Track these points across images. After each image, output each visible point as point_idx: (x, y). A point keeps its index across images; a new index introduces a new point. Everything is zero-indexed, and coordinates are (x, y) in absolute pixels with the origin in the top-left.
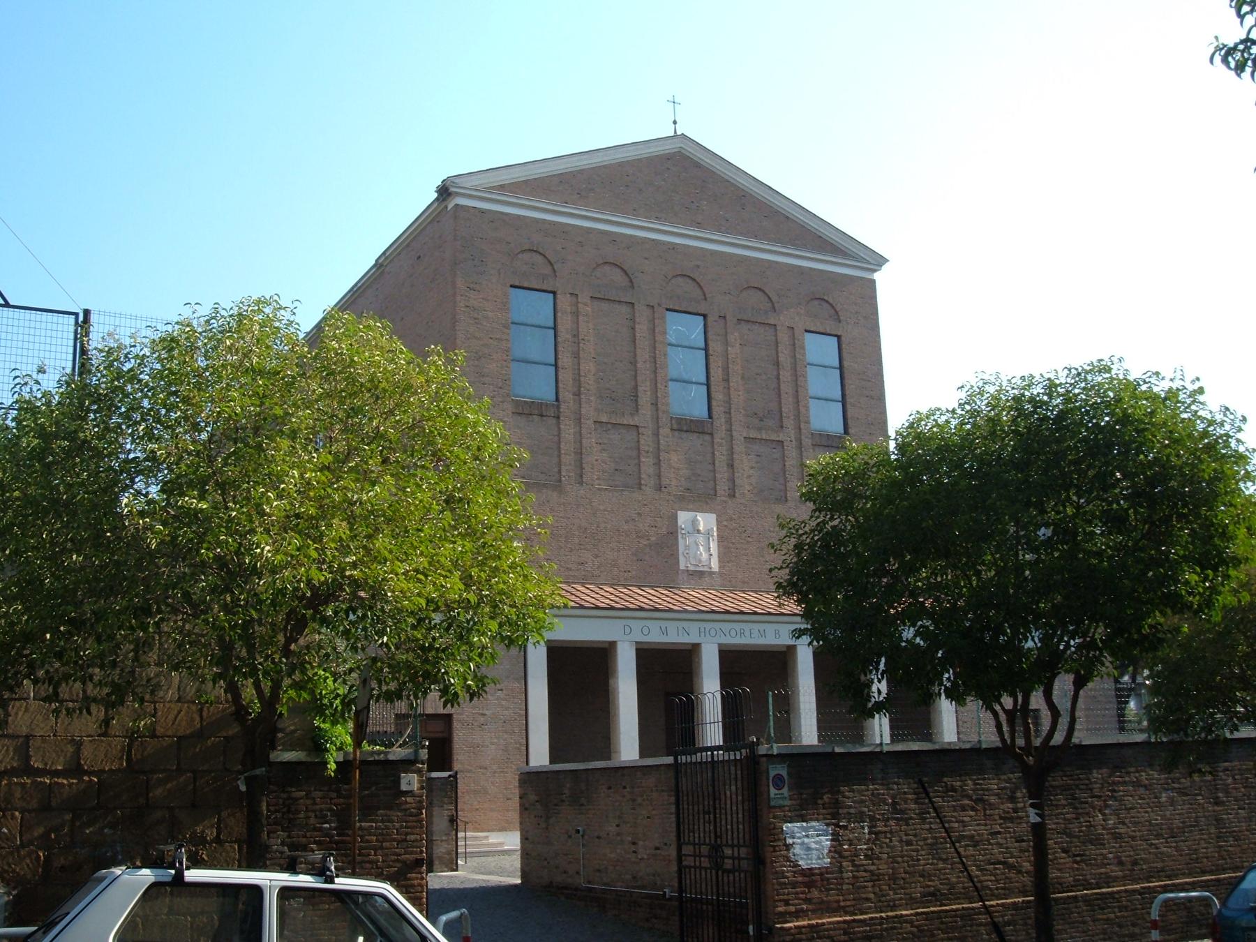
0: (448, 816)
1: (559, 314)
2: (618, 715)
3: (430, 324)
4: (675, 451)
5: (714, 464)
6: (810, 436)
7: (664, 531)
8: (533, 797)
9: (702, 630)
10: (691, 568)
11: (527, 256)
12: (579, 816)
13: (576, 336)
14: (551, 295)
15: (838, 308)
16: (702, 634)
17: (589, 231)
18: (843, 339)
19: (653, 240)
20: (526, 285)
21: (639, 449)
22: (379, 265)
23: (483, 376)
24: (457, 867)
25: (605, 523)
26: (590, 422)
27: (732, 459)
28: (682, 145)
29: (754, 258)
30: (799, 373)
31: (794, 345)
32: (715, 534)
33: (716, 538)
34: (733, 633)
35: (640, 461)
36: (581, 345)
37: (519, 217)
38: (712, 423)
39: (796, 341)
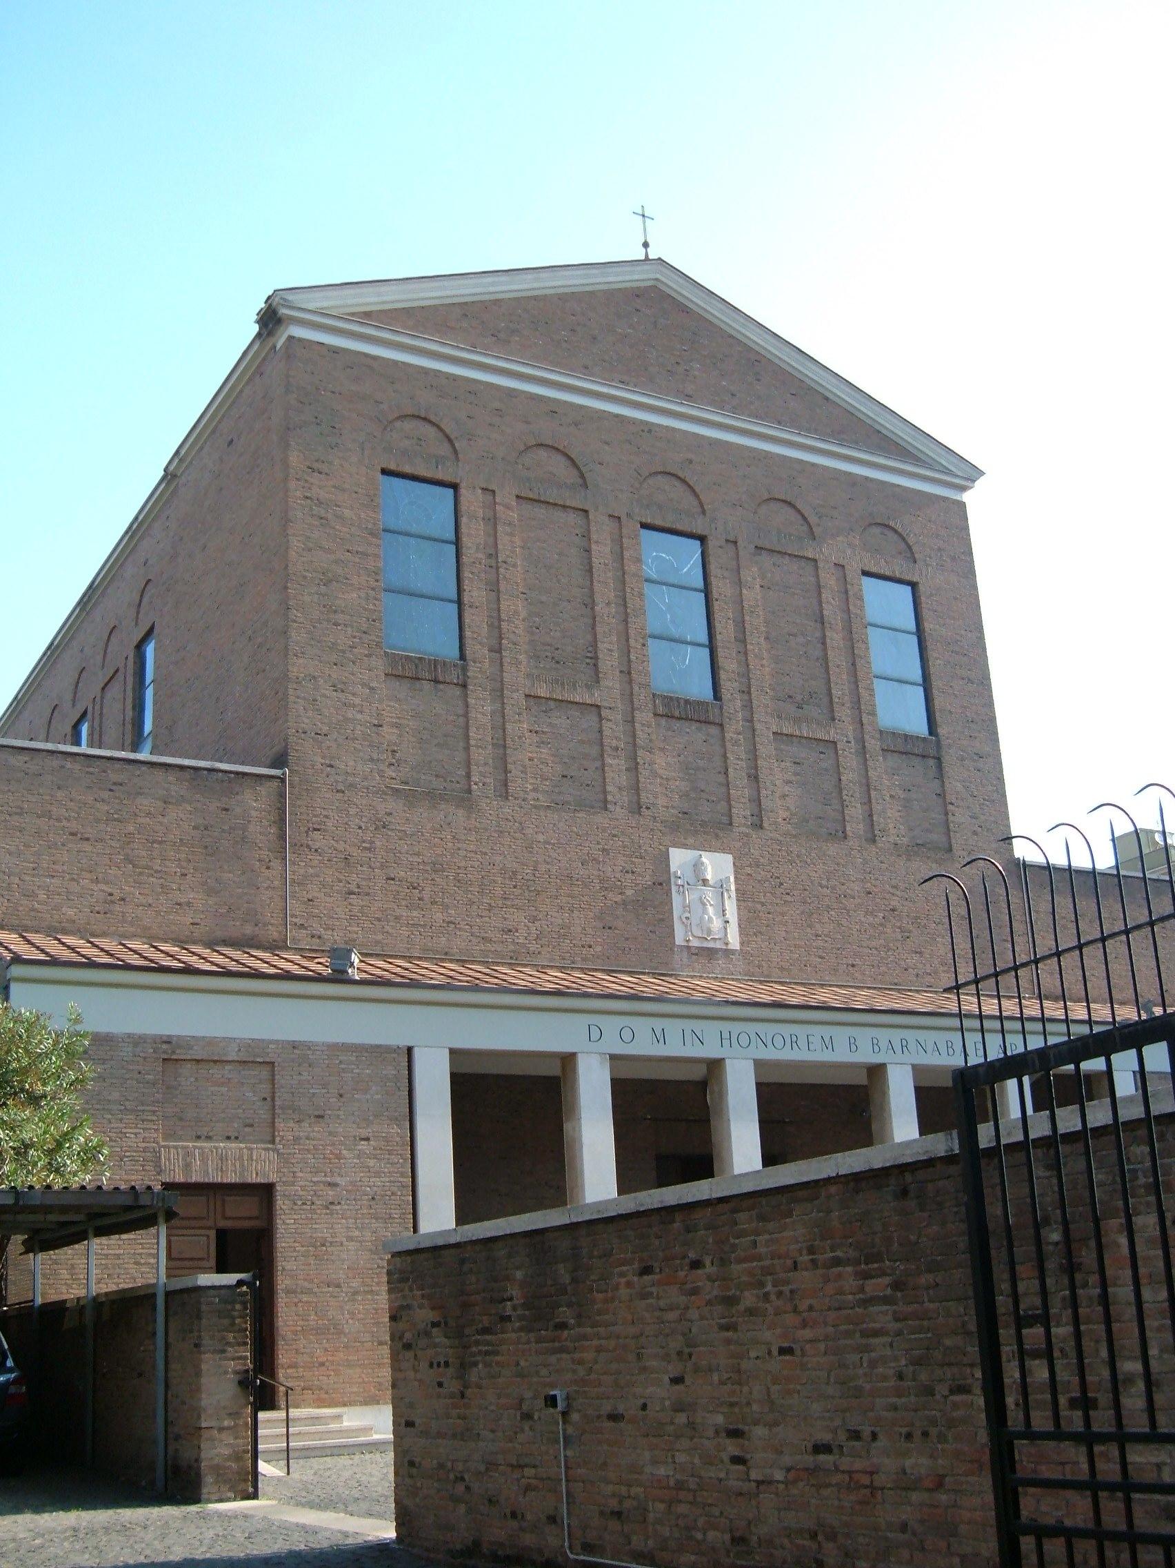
0: (236, 1373)
1: (464, 520)
2: (583, 1186)
3: (246, 540)
4: (662, 749)
5: (726, 773)
6: (878, 736)
7: (648, 880)
8: (424, 1315)
9: (726, 1035)
10: (695, 943)
11: (408, 425)
12: (553, 1359)
13: (493, 555)
14: (451, 491)
15: (911, 540)
16: (727, 1043)
17: (512, 393)
18: (921, 588)
19: (617, 416)
20: (407, 469)
21: (602, 745)
22: (169, 476)
23: (335, 612)
24: (256, 1487)
25: (548, 863)
26: (519, 697)
27: (756, 768)
28: (658, 276)
29: (778, 455)
30: (855, 636)
31: (846, 592)
32: (733, 887)
33: (733, 894)
34: (779, 1041)
35: (603, 765)
36: (502, 570)
37: (395, 363)
38: (721, 708)
39: (849, 587)
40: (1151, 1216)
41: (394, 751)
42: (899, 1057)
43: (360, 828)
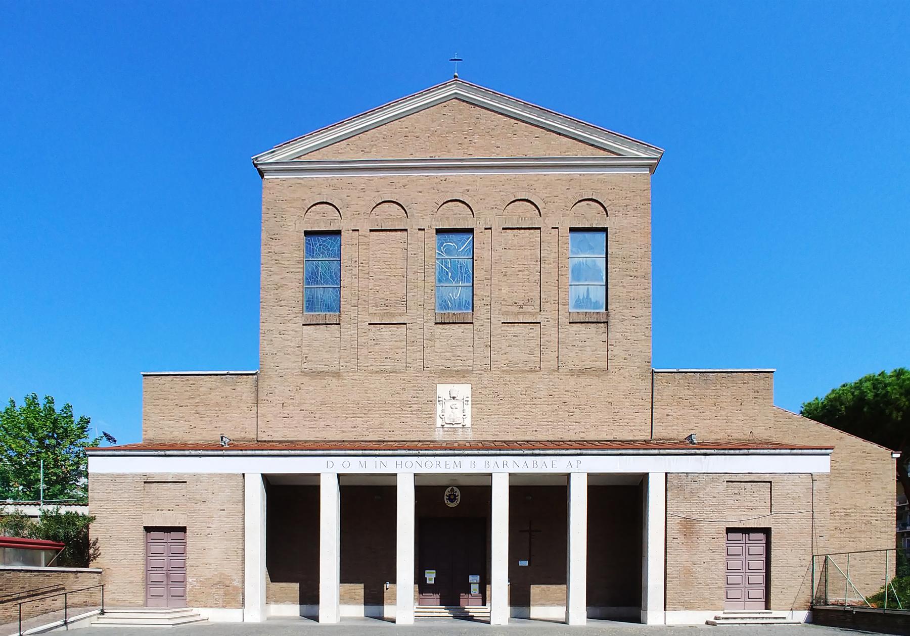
40: (88, 513)
41: (306, 357)
42: (501, 469)
43: (290, 391)
